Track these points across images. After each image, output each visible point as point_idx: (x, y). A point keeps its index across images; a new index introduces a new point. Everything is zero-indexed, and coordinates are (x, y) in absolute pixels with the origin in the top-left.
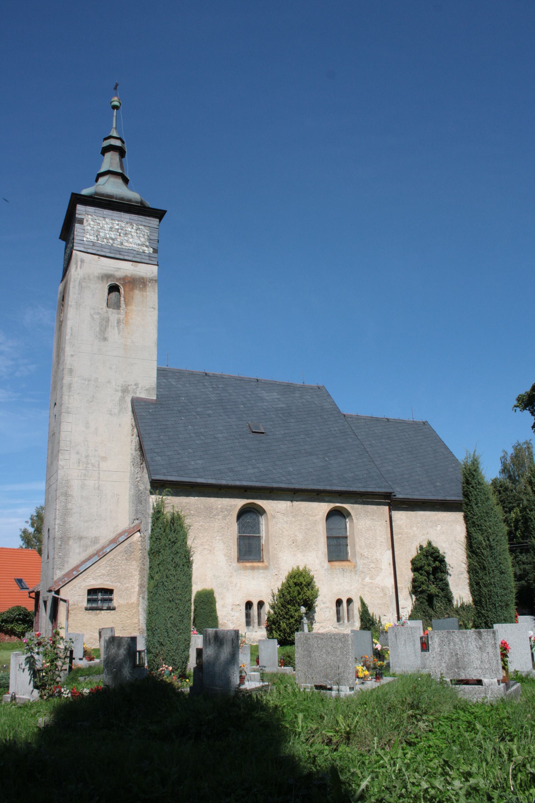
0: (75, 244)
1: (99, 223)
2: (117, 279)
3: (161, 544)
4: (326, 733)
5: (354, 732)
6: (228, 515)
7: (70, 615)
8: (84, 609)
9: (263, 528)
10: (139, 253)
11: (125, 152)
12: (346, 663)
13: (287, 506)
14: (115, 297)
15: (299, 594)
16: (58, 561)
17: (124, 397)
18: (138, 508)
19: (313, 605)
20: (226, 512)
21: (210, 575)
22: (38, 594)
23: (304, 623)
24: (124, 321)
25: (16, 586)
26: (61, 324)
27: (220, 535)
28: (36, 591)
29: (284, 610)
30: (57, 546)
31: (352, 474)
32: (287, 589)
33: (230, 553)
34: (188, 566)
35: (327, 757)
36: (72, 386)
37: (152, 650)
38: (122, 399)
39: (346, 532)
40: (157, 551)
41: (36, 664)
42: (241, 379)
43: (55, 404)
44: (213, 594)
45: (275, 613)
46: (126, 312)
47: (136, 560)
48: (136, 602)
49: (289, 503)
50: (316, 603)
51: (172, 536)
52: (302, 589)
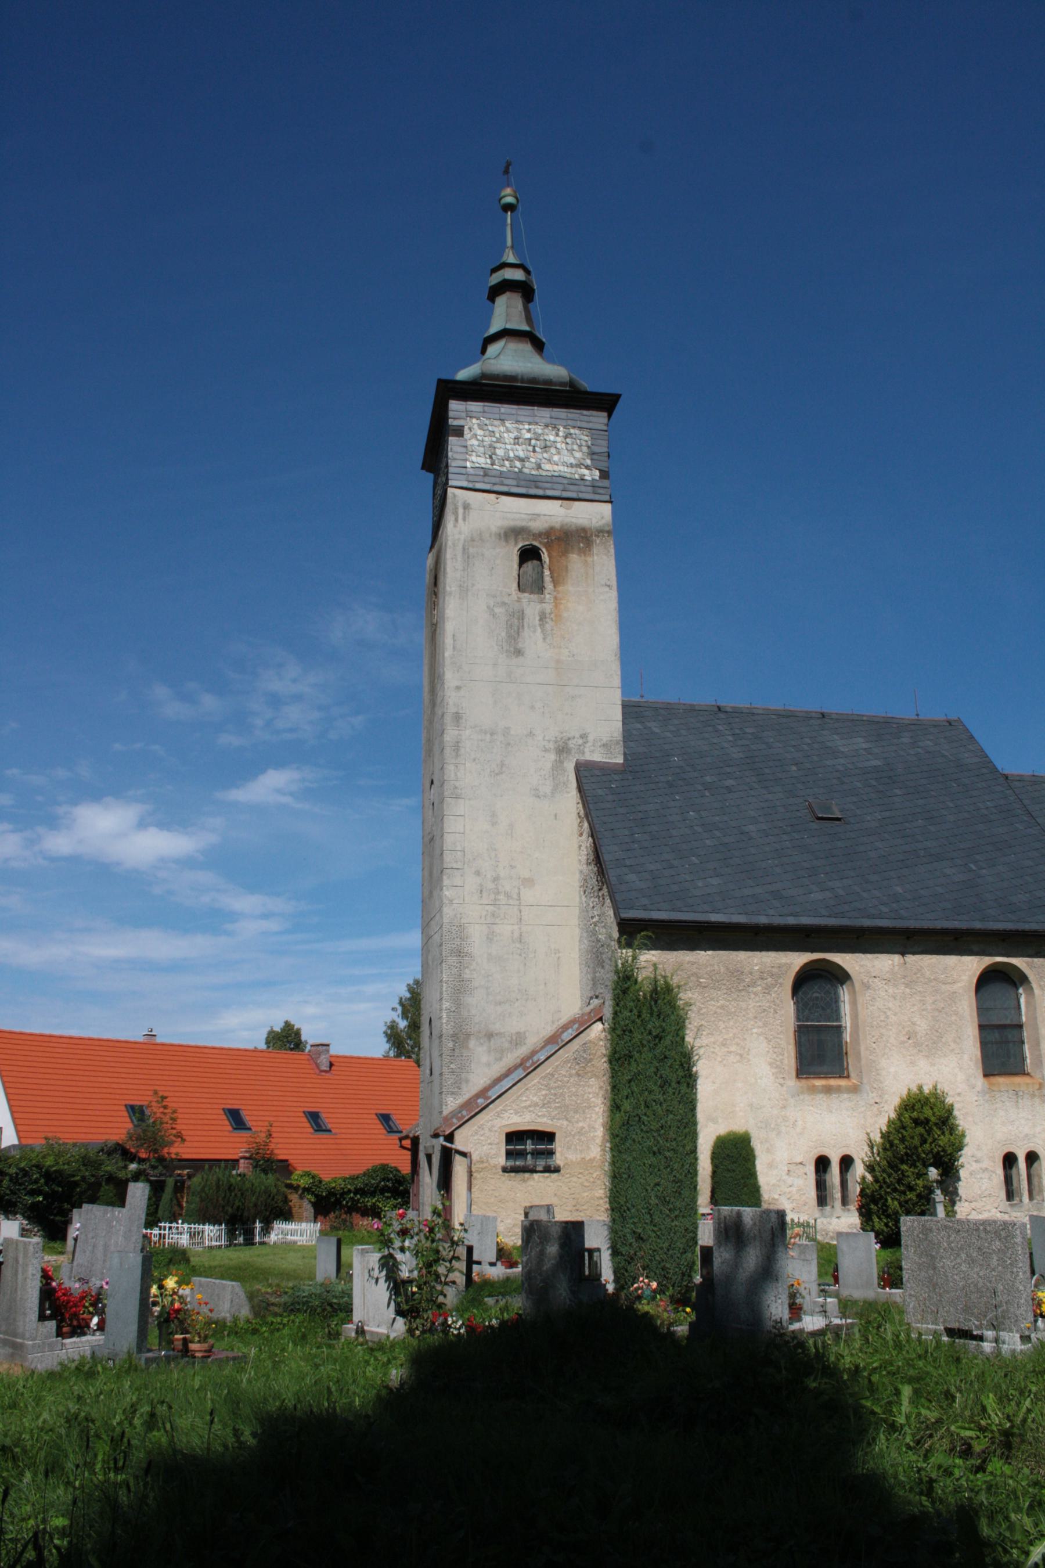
0: (450, 476)
1: (493, 432)
2: (534, 535)
3: (634, 1041)
4: (958, 1431)
5: (1022, 1432)
6: (774, 986)
7: (474, 1182)
8: (500, 1170)
9: (846, 1009)
10: (573, 482)
11: (533, 291)
12: (1011, 1284)
13: (893, 965)
14: (534, 569)
15: (924, 1142)
16: (449, 1080)
17: (561, 762)
18: (598, 975)
19: (953, 1164)
20: (770, 979)
21: (742, 1105)
22: (415, 1141)
23: (937, 1200)
24: (552, 616)
25: (379, 1128)
26: (434, 630)
27: (760, 1024)
28: (411, 1135)
29: (895, 1175)
30: (446, 1052)
31: (1027, 895)
32: (899, 1132)
33: (782, 1061)
34: (688, 1084)
35: (960, 1482)
36: (460, 745)
37: (622, 1249)
38: (558, 765)
39: (1020, 1014)
40: (625, 1055)
41: (398, 1269)
42: (790, 715)
43: (432, 782)
44: (750, 1142)
45: (876, 1180)
46: (556, 598)
47: (597, 1077)
48: (598, 1157)
49: (897, 958)
50: (961, 1160)
51: (654, 1024)
52: (929, 1132)
